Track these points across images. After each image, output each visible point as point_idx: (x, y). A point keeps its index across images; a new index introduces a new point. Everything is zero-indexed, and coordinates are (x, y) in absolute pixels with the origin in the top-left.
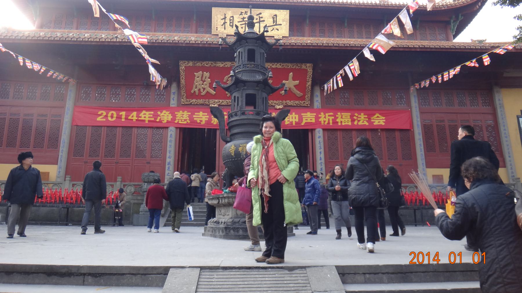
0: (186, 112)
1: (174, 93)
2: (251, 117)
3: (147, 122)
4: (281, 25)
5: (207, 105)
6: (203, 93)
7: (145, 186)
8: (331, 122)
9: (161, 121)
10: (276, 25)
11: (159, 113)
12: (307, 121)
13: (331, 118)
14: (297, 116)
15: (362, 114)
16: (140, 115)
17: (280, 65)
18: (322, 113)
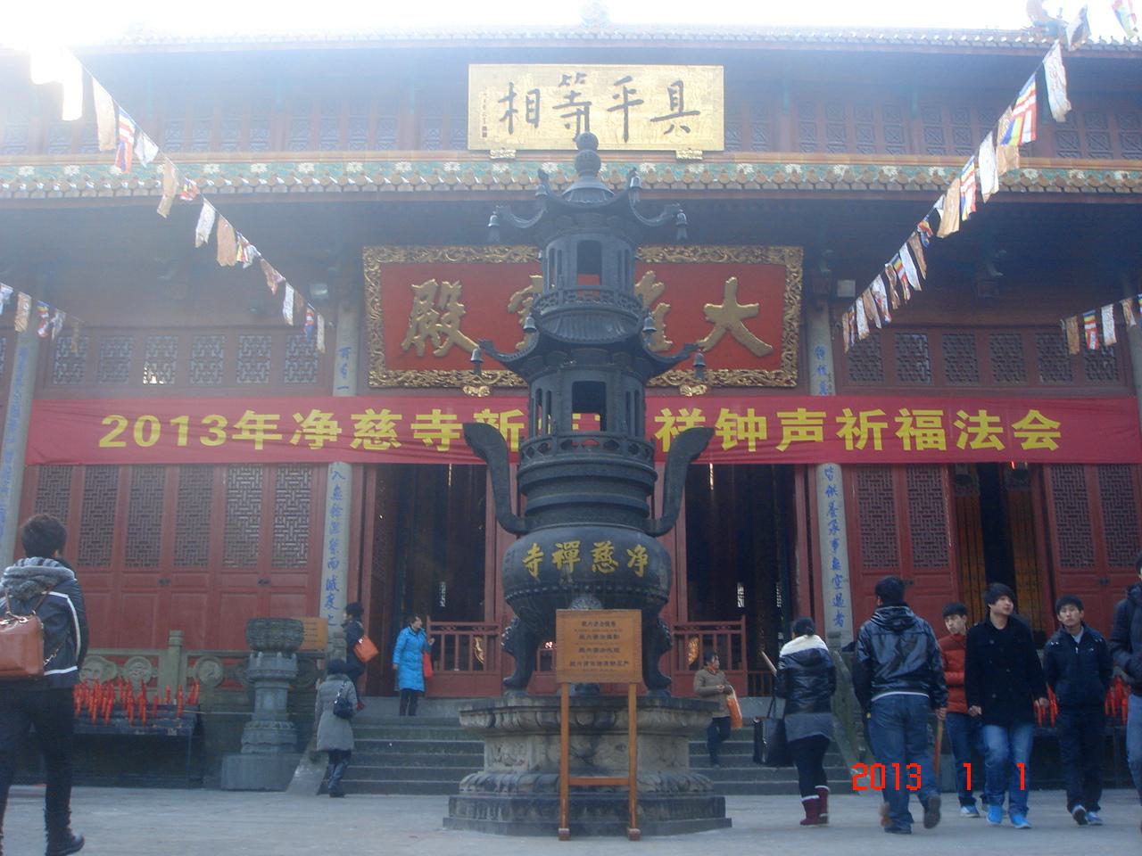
0: (385, 412)
1: (345, 352)
2: (590, 455)
3: (259, 447)
4: (697, 113)
5: (452, 387)
6: (441, 350)
7: (258, 661)
8: (877, 435)
9: (304, 444)
10: (681, 114)
11: (298, 417)
12: (796, 438)
13: (877, 427)
14: (762, 421)
15: (983, 413)
16: (237, 426)
17: (695, 252)
18: (847, 412)
